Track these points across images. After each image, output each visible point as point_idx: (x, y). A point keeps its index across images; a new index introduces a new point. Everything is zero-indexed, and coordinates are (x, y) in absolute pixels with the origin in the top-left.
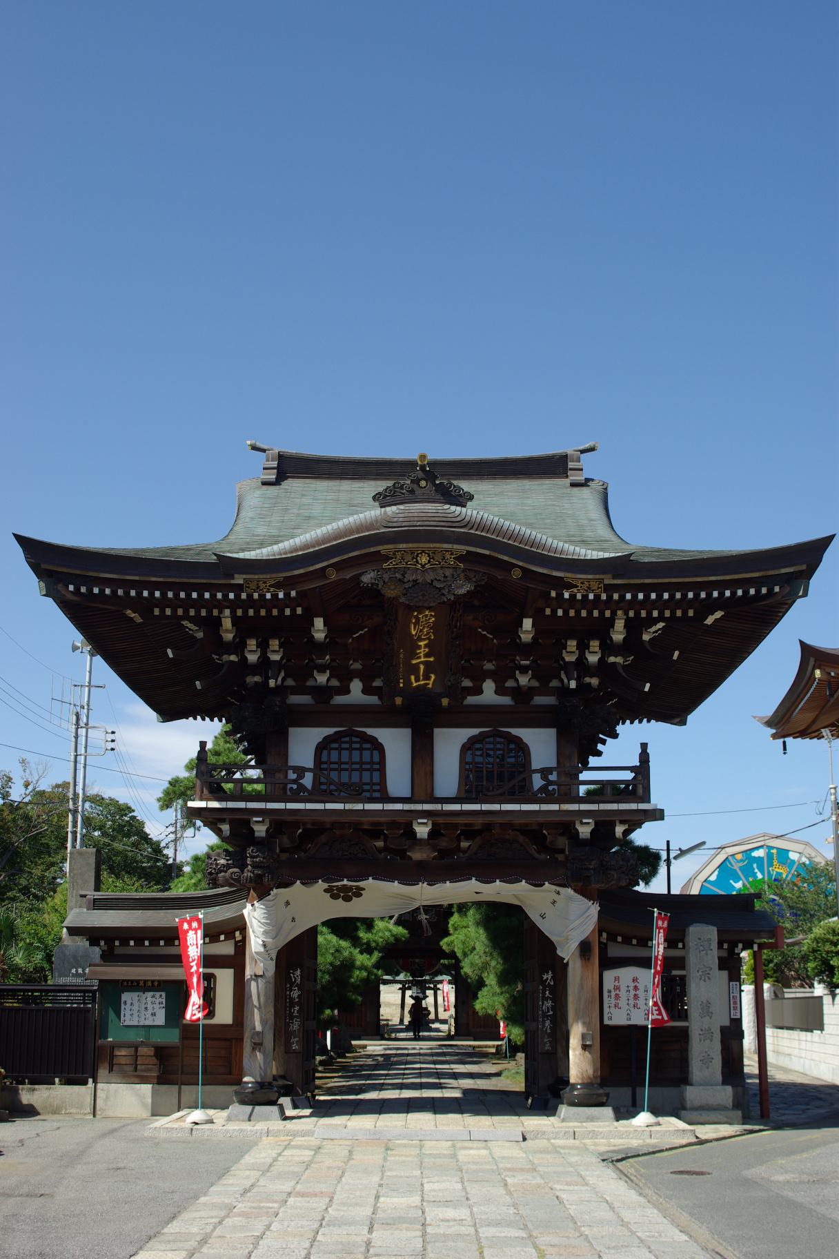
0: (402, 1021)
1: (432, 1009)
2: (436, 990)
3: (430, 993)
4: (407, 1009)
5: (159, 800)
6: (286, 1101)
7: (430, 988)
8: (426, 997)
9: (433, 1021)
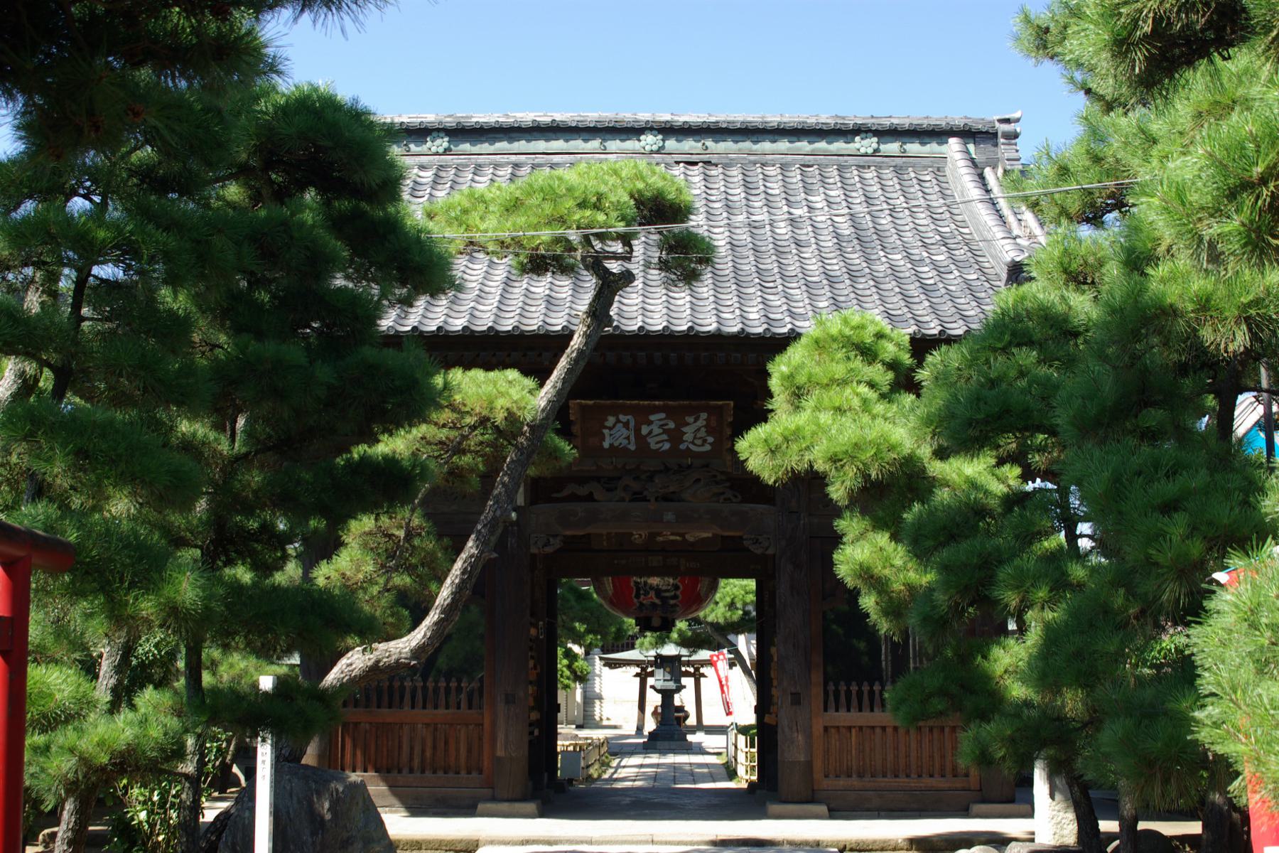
0: (640, 729)
1: (691, 708)
2: (698, 677)
3: (688, 682)
4: (649, 709)
5: (394, 452)
6: (104, 759)
7: (687, 674)
8: (680, 688)
9: (693, 730)
